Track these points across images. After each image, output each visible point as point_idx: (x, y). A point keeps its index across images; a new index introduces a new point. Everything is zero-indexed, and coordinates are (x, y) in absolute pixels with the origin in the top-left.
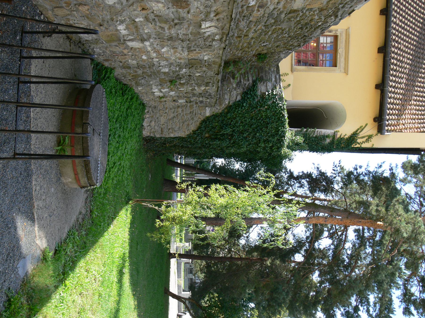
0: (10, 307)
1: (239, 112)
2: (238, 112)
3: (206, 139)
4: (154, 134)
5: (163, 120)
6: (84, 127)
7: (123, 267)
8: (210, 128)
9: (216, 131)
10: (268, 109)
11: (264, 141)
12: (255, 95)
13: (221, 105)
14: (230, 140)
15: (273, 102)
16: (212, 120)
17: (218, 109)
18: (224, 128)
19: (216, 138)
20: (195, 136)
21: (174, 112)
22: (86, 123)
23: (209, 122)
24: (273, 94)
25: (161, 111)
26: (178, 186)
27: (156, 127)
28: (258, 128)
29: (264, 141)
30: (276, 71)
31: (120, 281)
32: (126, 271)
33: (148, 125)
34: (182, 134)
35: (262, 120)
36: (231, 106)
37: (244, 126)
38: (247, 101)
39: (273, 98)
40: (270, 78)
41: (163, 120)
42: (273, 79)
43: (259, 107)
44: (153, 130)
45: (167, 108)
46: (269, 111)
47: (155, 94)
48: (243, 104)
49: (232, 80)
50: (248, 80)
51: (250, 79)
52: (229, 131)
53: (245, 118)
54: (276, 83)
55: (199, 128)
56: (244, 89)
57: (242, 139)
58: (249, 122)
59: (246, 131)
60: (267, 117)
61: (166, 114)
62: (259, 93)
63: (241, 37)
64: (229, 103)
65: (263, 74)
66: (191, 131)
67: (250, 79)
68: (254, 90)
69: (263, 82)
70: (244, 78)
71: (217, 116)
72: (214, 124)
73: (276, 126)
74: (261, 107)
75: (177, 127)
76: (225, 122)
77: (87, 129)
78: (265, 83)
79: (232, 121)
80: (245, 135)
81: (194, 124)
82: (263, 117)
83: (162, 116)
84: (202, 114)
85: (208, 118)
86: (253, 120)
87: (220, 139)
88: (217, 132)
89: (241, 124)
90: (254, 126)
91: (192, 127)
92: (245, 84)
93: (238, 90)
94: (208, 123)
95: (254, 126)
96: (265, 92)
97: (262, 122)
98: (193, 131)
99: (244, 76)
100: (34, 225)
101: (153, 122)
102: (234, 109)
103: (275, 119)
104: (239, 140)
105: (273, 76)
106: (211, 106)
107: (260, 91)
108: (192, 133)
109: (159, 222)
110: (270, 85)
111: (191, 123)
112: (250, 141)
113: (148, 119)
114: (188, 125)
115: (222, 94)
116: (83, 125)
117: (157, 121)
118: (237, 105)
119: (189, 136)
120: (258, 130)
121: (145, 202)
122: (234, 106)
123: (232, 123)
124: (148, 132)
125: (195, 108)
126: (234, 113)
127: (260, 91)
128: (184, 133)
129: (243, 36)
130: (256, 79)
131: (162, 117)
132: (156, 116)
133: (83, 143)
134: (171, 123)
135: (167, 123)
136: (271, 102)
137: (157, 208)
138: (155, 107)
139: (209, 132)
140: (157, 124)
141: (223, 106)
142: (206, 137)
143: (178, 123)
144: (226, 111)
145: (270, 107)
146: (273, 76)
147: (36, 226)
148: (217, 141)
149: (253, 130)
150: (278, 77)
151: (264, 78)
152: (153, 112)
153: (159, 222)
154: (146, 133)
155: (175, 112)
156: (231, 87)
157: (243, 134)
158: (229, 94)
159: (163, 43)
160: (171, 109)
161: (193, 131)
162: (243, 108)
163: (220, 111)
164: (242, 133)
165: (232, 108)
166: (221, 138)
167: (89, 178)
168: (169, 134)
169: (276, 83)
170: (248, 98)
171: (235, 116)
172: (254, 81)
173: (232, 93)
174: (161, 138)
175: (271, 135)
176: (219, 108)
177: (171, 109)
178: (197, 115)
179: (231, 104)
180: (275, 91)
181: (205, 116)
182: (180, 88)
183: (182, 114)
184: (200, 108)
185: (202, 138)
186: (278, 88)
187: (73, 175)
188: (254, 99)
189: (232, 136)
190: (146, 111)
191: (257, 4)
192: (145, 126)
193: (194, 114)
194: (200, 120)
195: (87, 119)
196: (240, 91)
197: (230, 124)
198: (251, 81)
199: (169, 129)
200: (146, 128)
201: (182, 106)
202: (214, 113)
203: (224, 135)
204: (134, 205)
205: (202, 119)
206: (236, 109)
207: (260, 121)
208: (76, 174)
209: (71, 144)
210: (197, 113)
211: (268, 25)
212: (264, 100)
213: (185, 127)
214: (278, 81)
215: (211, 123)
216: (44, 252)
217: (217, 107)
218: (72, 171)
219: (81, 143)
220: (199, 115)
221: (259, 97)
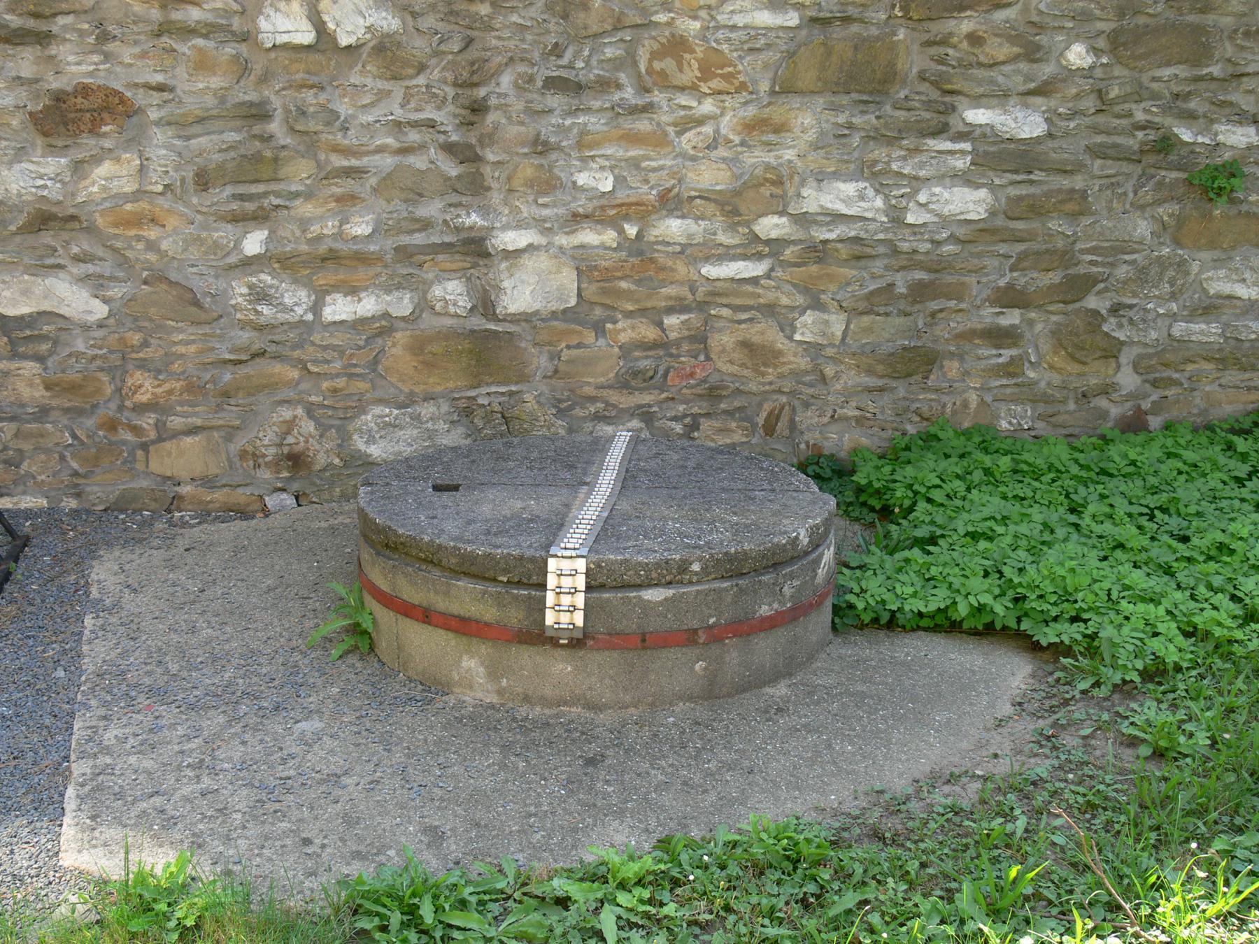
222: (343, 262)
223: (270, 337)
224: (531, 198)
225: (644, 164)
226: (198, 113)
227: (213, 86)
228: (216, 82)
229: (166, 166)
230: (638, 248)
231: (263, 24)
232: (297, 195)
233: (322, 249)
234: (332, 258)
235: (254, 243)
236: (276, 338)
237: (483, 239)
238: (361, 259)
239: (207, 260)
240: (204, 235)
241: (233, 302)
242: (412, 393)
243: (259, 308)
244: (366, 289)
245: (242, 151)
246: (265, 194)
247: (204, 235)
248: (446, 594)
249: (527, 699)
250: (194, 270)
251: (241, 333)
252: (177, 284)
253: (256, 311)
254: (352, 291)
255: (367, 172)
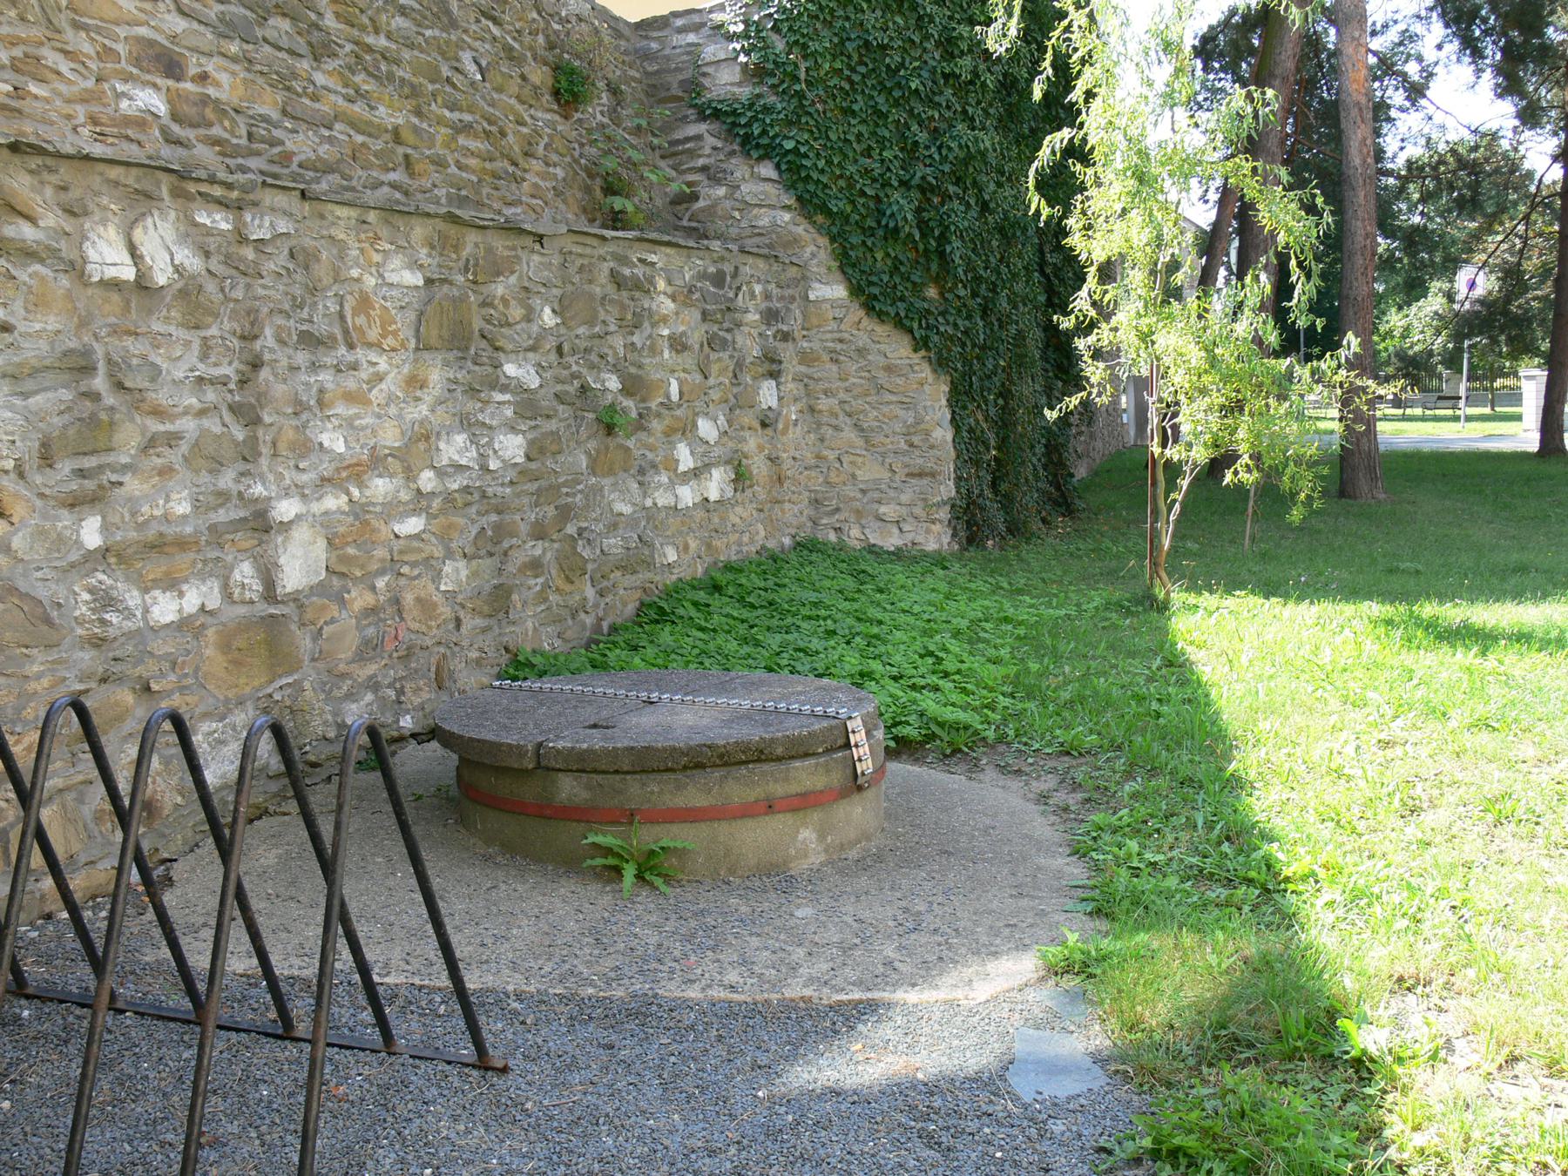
0: (1185, 1155)
1: (821, 164)
2: (822, 171)
3: (949, 296)
4: (938, 505)
5: (869, 471)
6: (553, 764)
7: (1430, 626)
8: (898, 280)
9: (912, 255)
10: (805, 46)
11: (949, 56)
12: (752, 105)
13: (796, 241)
14: (946, 197)
15: (776, 29)
16: (863, 272)
17: (815, 249)
18: (892, 225)
19: (942, 255)
20: (936, 338)
21: (836, 428)
22: (538, 755)
23: (871, 284)
24: (745, 35)
25: (833, 477)
26: (1099, 394)
27: (904, 498)
28: (888, 85)
29: (949, 56)
30: (660, 29)
31: (1484, 639)
32: (1453, 613)
33: (896, 531)
34: (933, 396)
35: (853, 70)
36: (799, 199)
37: (882, 142)
38: (776, 135)
39: (758, 31)
40: (688, 53)
41: (869, 471)
42: (691, 38)
43: (797, 87)
44: (918, 511)
45: (818, 457)
46: (813, 46)
47: (714, 495)
48: (789, 151)
49: (701, 204)
50: (699, 137)
51: (693, 129)
52: (902, 205)
53: (846, 141)
54: (703, 25)
55: (899, 324)
56: (732, 153)
57: (940, 148)
58: (864, 121)
59: (902, 130)
60: (838, 51)
61: (845, 459)
62: (745, 92)
63: (406, 156)
64: (787, 208)
65: (674, 81)
66: (916, 358)
67: (693, 129)
68: (734, 113)
69: (704, 80)
70: (692, 154)
71: (845, 255)
72: (879, 265)
73: (879, 13)
74: (796, 79)
75: (901, 413)
76: (870, 222)
77: (558, 751)
78: (705, 69)
79: (863, 193)
80: (923, 137)
81: (882, 347)
82: (838, 65)
83: (854, 476)
84: (839, 313)
85: (856, 291)
86: (856, 107)
87: (943, 239)
88: (917, 251)
89: (875, 154)
90: (881, 100)
91: (895, 355)
92: (715, 148)
93: (738, 174)
94: (875, 290)
95: (881, 100)
96: (738, 68)
97: (862, 69)
98: (915, 351)
99: (684, 157)
100: (889, 1005)
101: (883, 509)
102: (811, 187)
103: (848, 18)
104: (944, 159)
105: (678, 40)
106: (804, 278)
107: (736, 90)
108: (923, 353)
109: (1236, 473)
110: (712, 51)
111: (882, 359)
112: (948, 114)
113: (867, 531)
114: (889, 369)
115: (757, 240)
116: (548, 769)
117: (876, 495)
118: (794, 174)
119: (941, 363)
120: (899, 85)
121: (1155, 536)
122: (800, 186)
123: (869, 192)
124: (928, 531)
125: (816, 345)
126: (826, 186)
127: (736, 90)
128: (926, 387)
129: (401, 150)
130: (692, 106)
131: (858, 473)
132: (854, 499)
133: (617, 772)
134: (882, 439)
135: (883, 455)
136: (775, 37)
137: (1185, 483)
138: (816, 502)
139: (914, 284)
140: (892, 493)
141: (800, 230)
142: (942, 294)
143: (885, 409)
144: (820, 218)
145: (796, 42)
146: (678, 40)
147: (900, 995)
148: (948, 249)
149: (897, 104)
150: (679, 22)
151: (687, 75)
152: (838, 510)
153: (1236, 473)
154: (937, 538)
155: (834, 422)
156: (728, 204)
157: (916, 143)
158: (755, 211)
159: (282, 448)
160: (822, 440)
161: (915, 351)
162: (803, 150)
163: (824, 241)
164: (911, 151)
165: (807, 196)
166: (937, 233)
167: (799, 750)
168: (932, 447)
169: (703, 25)
170: (764, 133)
171: (842, 183)
172: (702, 117)
173: (747, 199)
174: (959, 479)
175: (920, 28)
176: (810, 249)
177: (822, 440)
178: (846, 336)
179: (790, 200)
180: (732, 28)
181: (847, 303)
182: (668, 397)
183: (842, 395)
184: (815, 321)
185: (942, 314)
186: (718, 17)
187: (777, 824)
188: (767, 109)
189: (926, 188)
190: (832, 537)
191: (159, 81)
192: (900, 543)
193: (839, 347)
194: (866, 322)
195: (519, 750)
196: (739, 168)
197: (878, 199)
198: (702, 128)
199: (911, 445)
200: (910, 537)
201: (808, 395)
202: (835, 264)
203: (923, 225)
204: (1170, 575)
205: (862, 313)
206: (808, 177)
207: (857, 78)
208: (770, 807)
209: (621, 824)
210: (837, 335)
211: (310, 44)
212: (770, 66)
213: (900, 381)
214: (696, 19)
215: (874, 279)
216: (1056, 971)
217: (807, 255)
218: (750, 823)
219: (618, 777)
220: (843, 327)
221: (757, 91)
222: (166, 549)
223: (111, 655)
224: (292, 463)
225: (357, 422)
226: (34, 362)
227: (49, 328)
228: (53, 323)
229: (12, 433)
230: (359, 510)
231: (92, 254)
232: (126, 468)
233: (151, 534)
234: (158, 546)
235: (91, 534)
236: (118, 653)
237: (266, 511)
238: (182, 544)
239: (50, 560)
240: (48, 525)
241: (77, 613)
242: (227, 700)
243: (107, 616)
244: (186, 581)
245: (76, 413)
246: (101, 468)
247: (48, 525)
248: (786, 779)
249: (842, 847)
250: (39, 574)
251: (81, 654)
252: (27, 595)
253: (103, 622)
254: (172, 584)
255: (181, 438)
